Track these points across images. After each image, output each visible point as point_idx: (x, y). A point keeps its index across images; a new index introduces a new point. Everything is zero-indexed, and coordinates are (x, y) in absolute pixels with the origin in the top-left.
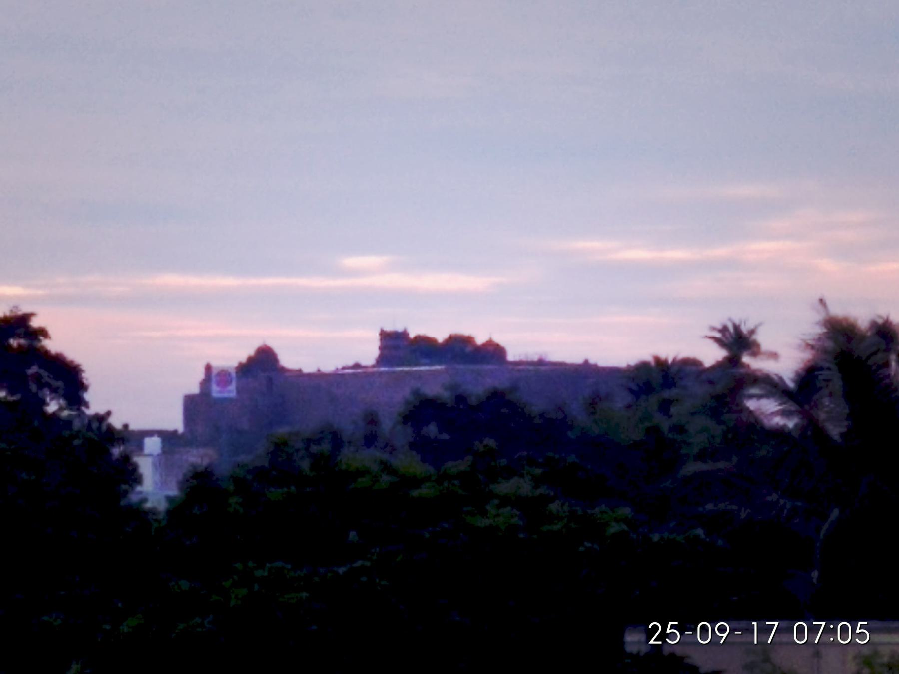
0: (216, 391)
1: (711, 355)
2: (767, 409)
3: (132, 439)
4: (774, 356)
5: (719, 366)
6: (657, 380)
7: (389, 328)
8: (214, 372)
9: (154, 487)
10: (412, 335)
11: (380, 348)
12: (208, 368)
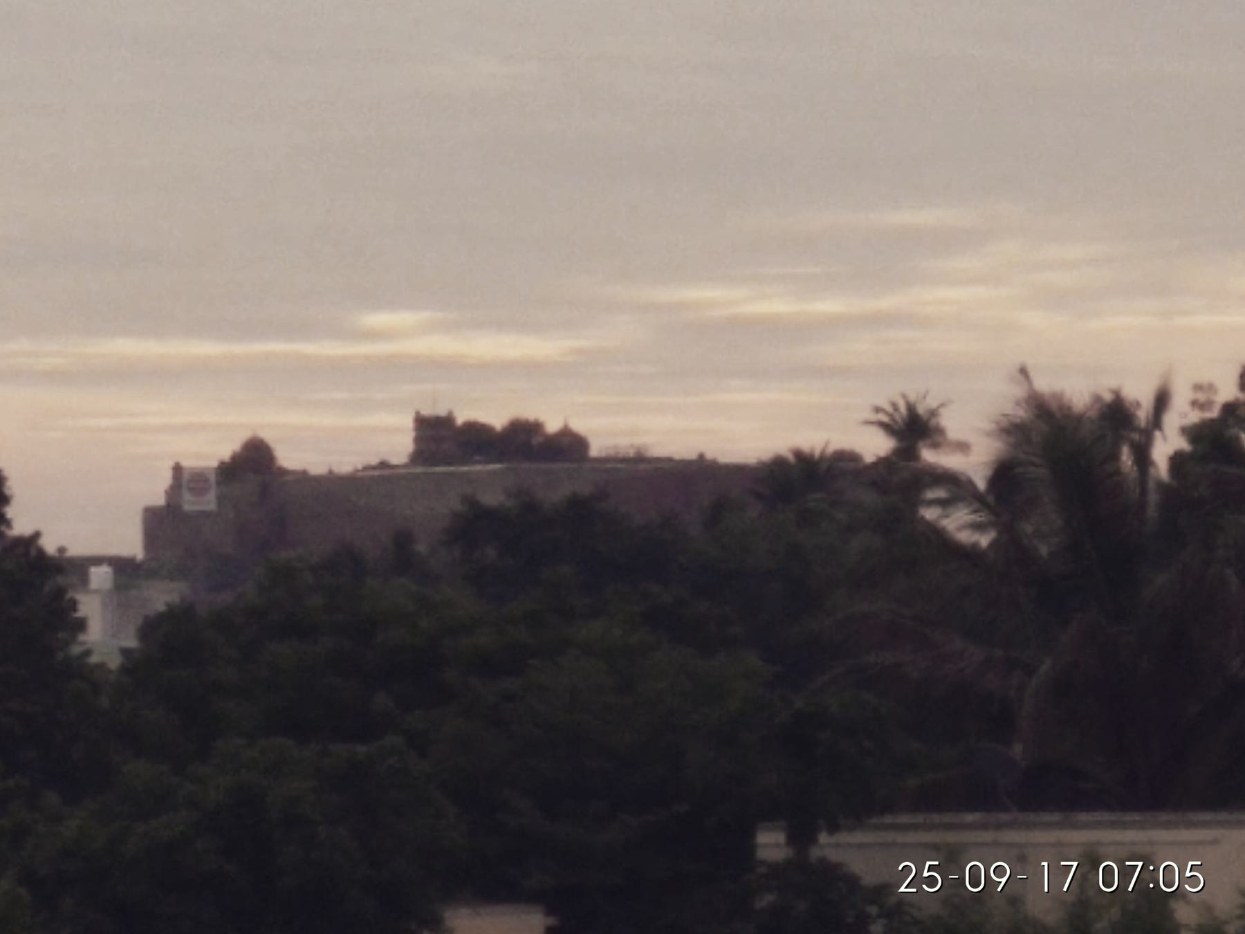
0: (190, 504)
1: (875, 446)
2: (959, 524)
3: (70, 569)
4: (963, 447)
5: (883, 462)
6: (799, 480)
7: (427, 411)
8: (186, 476)
9: (103, 630)
10: (460, 420)
11: (417, 440)
12: (177, 469)
